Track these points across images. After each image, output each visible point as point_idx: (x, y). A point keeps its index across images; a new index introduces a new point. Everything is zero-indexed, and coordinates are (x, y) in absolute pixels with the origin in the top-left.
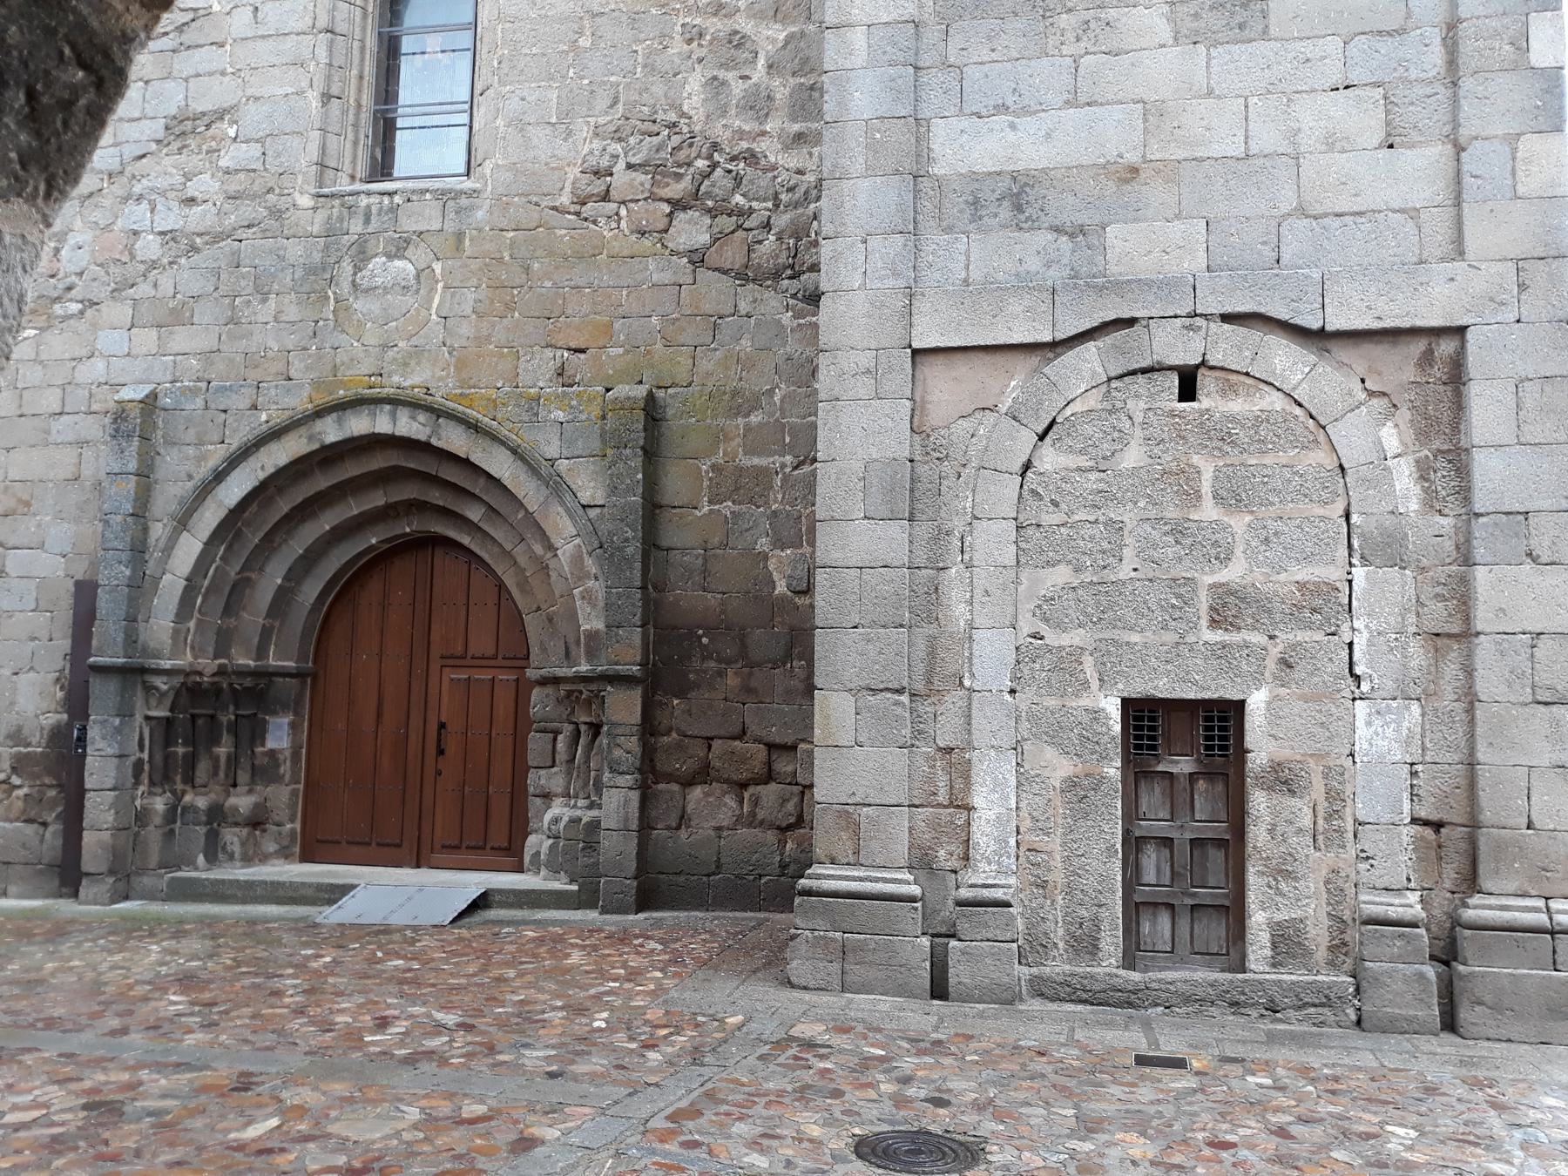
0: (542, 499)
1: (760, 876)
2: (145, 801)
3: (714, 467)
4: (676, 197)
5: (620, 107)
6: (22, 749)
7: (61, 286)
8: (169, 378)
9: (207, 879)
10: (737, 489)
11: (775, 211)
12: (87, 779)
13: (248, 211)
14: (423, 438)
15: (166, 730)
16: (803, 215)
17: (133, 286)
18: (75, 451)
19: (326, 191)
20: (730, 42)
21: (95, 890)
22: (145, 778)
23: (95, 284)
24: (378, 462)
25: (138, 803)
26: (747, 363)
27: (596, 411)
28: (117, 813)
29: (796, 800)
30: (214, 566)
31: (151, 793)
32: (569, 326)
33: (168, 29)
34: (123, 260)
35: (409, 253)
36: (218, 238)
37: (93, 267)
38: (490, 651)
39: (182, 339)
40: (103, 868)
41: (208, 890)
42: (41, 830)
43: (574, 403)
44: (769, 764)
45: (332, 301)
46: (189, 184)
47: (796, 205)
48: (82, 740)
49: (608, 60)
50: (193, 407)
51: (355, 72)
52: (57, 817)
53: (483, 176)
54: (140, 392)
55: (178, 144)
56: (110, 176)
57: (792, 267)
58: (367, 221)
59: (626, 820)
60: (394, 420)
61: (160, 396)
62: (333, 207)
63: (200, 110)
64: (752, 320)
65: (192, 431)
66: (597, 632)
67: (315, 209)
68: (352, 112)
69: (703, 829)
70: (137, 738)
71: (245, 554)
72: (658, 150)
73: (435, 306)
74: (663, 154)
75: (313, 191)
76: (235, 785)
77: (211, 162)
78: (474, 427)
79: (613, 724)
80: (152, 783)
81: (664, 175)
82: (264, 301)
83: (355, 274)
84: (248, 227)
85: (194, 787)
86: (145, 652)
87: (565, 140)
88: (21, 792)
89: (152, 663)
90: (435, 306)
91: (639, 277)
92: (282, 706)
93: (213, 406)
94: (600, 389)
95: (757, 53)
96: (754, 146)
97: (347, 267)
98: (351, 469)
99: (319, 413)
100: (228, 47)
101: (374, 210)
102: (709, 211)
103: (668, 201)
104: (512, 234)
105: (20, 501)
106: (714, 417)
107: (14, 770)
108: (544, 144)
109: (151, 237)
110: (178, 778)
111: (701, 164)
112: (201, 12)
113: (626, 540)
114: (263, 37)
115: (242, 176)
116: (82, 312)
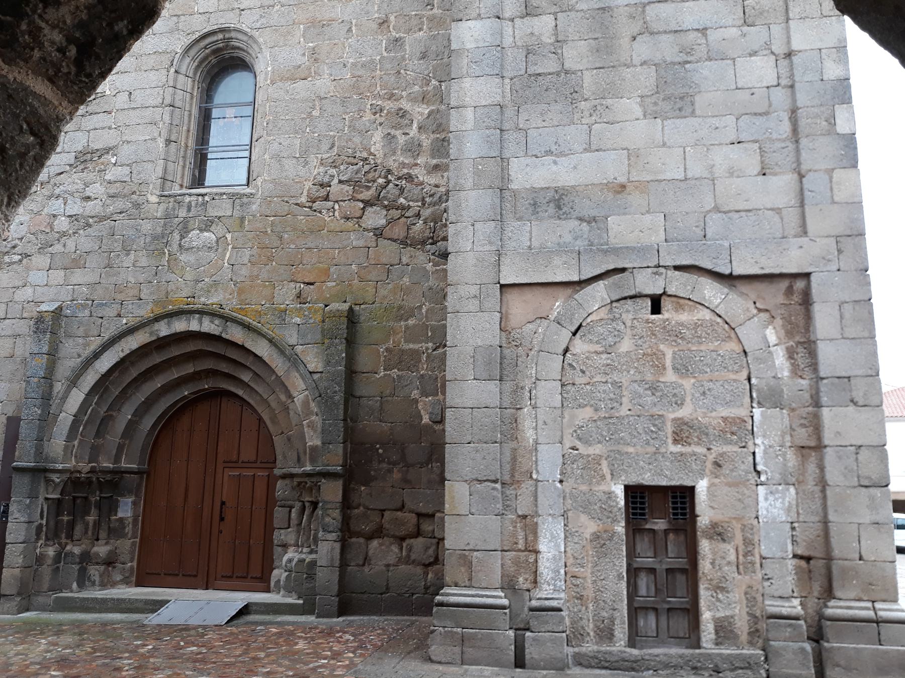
0: (286, 368)
1: (413, 594)
2: (42, 550)
3: (387, 350)
5: (335, 148)
8: (70, 298)
9: (78, 598)
10: (401, 362)
12: (7, 537)
13: (120, 204)
14: (217, 333)
15: (57, 506)
16: (438, 209)
17: (51, 245)
18: (12, 340)
19: (166, 193)
20: (398, 114)
23: (30, 244)
25: (38, 551)
26: (407, 291)
27: (319, 317)
28: (25, 557)
29: (434, 547)
34: (47, 231)
36: (101, 219)
38: (253, 458)
39: (78, 277)
40: (14, 592)
43: (306, 313)
44: (418, 526)
45: (167, 255)
46: (87, 189)
49: (329, 123)
51: (185, 128)
53: (257, 186)
55: (82, 167)
57: (432, 238)
58: (189, 210)
59: (332, 560)
60: (201, 323)
62: (169, 202)
65: (81, 329)
67: (159, 203)
68: (182, 149)
69: (378, 566)
71: (110, 400)
72: (356, 173)
73: (227, 258)
74: (359, 175)
75: (158, 193)
76: (97, 540)
78: (247, 327)
79: (325, 502)
80: (47, 539)
81: (360, 186)
82: (128, 255)
83: (181, 240)
84: (120, 213)
85: (73, 541)
86: (47, 459)
87: (304, 167)
89: (51, 466)
90: (227, 258)
91: (345, 243)
93: (95, 314)
94: (322, 305)
95: (412, 121)
96: (411, 171)
97: (176, 236)
99: (157, 319)
100: (113, 114)
101: (193, 204)
102: (385, 207)
103: (362, 201)
104: (272, 218)
108: (291, 169)
110: (63, 536)
111: (381, 181)
113: (335, 392)
114: (134, 108)
115: (118, 185)
116: (20, 261)
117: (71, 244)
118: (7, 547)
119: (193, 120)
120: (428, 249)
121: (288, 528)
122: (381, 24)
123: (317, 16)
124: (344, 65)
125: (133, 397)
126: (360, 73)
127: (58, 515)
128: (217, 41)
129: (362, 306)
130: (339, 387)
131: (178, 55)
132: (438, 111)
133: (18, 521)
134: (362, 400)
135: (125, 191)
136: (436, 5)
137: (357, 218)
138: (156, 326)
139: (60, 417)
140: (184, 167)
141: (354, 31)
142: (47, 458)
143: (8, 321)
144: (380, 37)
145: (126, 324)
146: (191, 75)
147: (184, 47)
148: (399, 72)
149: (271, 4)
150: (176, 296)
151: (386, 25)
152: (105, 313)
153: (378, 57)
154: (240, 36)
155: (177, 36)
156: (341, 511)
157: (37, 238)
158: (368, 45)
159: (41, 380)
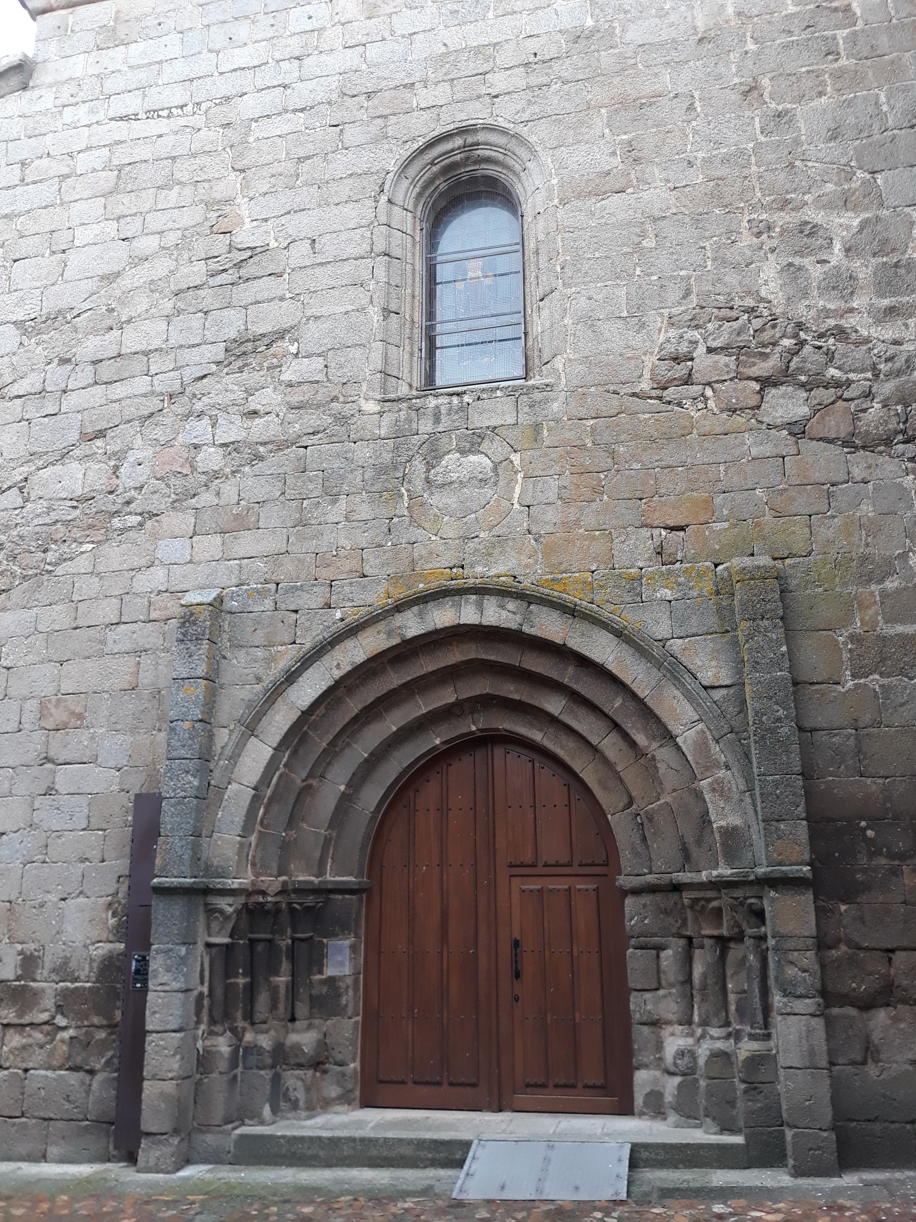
0: (653, 683)
2: (208, 1043)
3: (852, 638)
4: (765, 374)
6: (69, 984)
7: (120, 500)
8: (235, 581)
9: (283, 1137)
10: (883, 660)
11: (875, 381)
12: (148, 1020)
13: (312, 419)
14: (513, 626)
16: (907, 382)
17: (194, 495)
19: (392, 396)
20: (802, 232)
21: (158, 1154)
22: (205, 1019)
23: (156, 496)
24: (454, 656)
25: (200, 1044)
26: (873, 528)
27: (708, 586)
28: (182, 1058)
30: (277, 774)
31: (211, 1033)
32: (664, 504)
33: (226, 267)
34: (185, 472)
35: (485, 446)
36: (281, 446)
37: (153, 481)
38: (565, 859)
39: (246, 543)
41: (284, 1150)
42: (88, 1078)
43: (681, 580)
45: (406, 498)
46: (250, 398)
47: (898, 373)
48: (142, 973)
49: (675, 257)
50: (262, 608)
51: (409, 291)
52: (108, 1062)
53: (556, 370)
54: (209, 596)
55: (239, 363)
56: (171, 397)
57: (903, 432)
58: (437, 419)
59: (812, 1053)
60: (480, 608)
61: (226, 600)
63: (261, 332)
64: (870, 486)
66: (735, 829)
67: (381, 414)
70: (199, 969)
71: (313, 757)
72: (738, 334)
73: (516, 495)
74: (744, 337)
75: (379, 397)
76: (293, 1019)
77: (272, 378)
78: (570, 611)
80: (213, 1021)
82: (334, 502)
83: (428, 471)
84: (313, 434)
85: (253, 1024)
86: (208, 870)
88: (66, 1035)
89: (218, 883)
90: (516, 495)
91: (737, 452)
92: (344, 927)
93: (283, 606)
95: (831, 239)
96: (842, 322)
97: (419, 465)
98: (427, 665)
99: (400, 607)
100: (286, 276)
101: (443, 410)
102: (803, 385)
103: (756, 379)
104: (592, 422)
105: (73, 713)
106: (845, 584)
107: (59, 1009)
109: (213, 449)
110: (239, 1014)
111: (787, 342)
112: (259, 250)
113: (779, 720)
114: (322, 264)
115: (305, 387)
116: (141, 524)
117: (229, 490)
118: (149, 1038)
119: (417, 279)
120: (900, 452)
121: (657, 989)
122: (746, 93)
123: (629, 92)
124: (689, 162)
125: (347, 751)
126: (719, 173)
127: (227, 975)
128: (452, 150)
129: (788, 561)
130: (784, 709)
131: (391, 175)
132: (878, 219)
133: (167, 988)
134: (818, 735)
135: (319, 397)
136: (842, 54)
137: (752, 408)
138: (399, 620)
139: (228, 793)
140: (412, 354)
141: (699, 109)
142: (207, 868)
143: (123, 626)
144: (747, 113)
145: (342, 620)
146: (410, 208)
147: (399, 163)
148: (791, 165)
149: (545, 82)
150: (430, 566)
151: (755, 94)
152: (301, 602)
153: (752, 145)
154: (493, 138)
155: (387, 146)
156: (817, 954)
157: (168, 486)
158: (728, 128)
159: (197, 725)
